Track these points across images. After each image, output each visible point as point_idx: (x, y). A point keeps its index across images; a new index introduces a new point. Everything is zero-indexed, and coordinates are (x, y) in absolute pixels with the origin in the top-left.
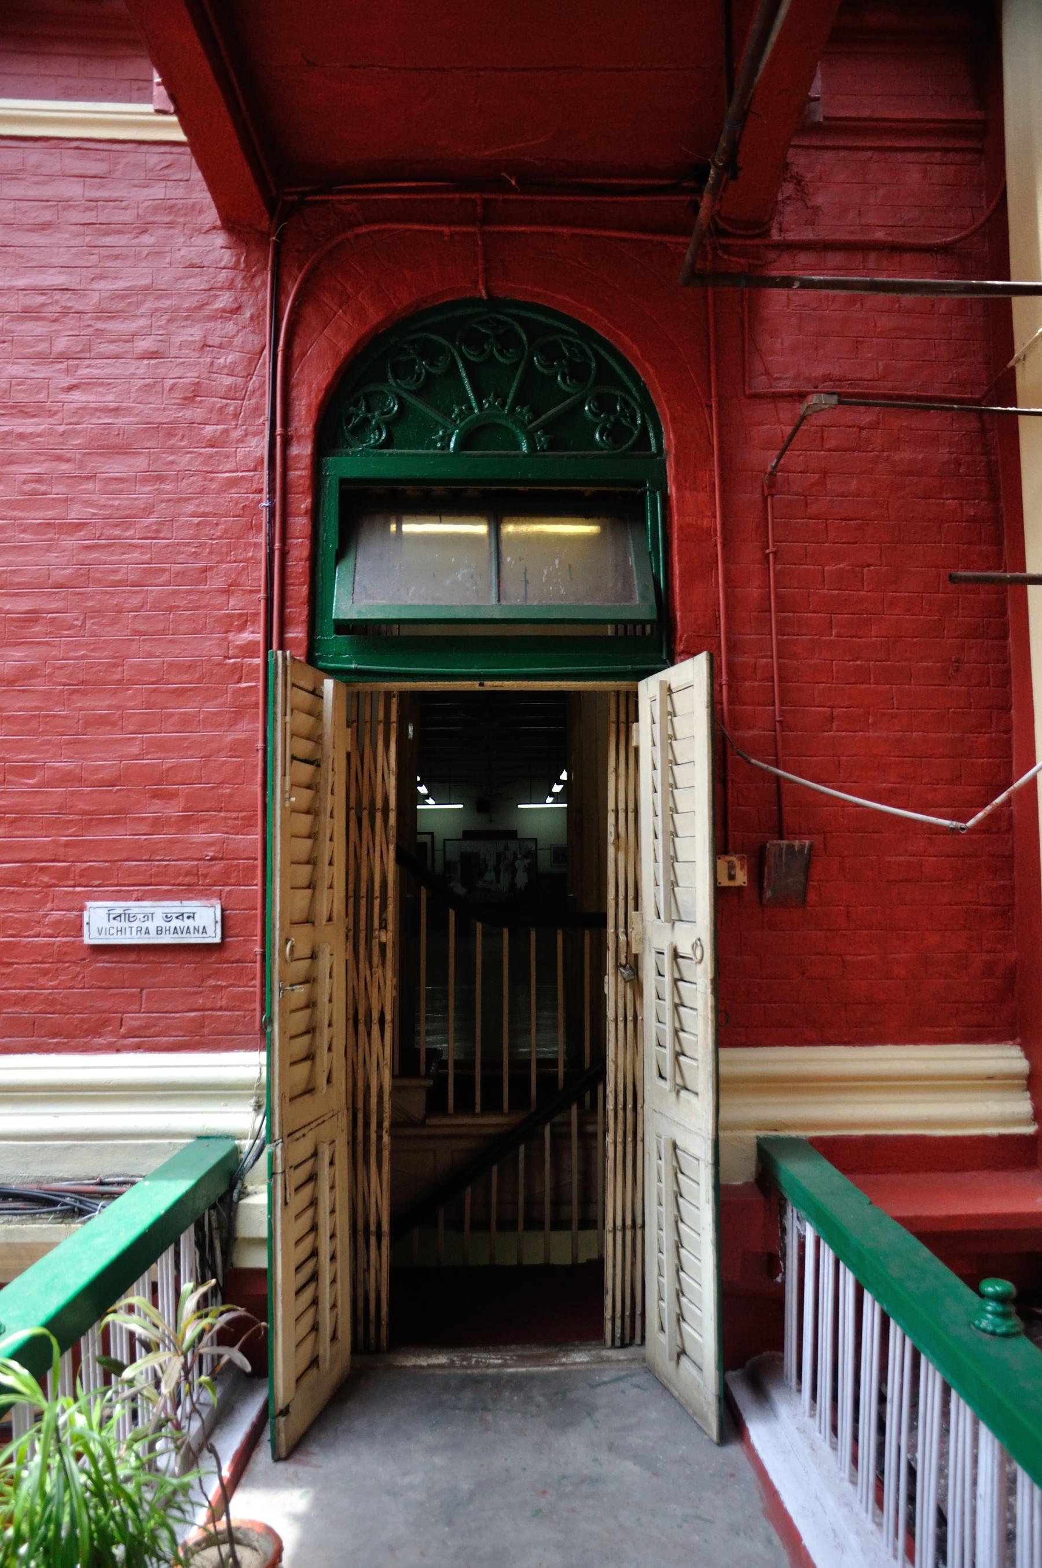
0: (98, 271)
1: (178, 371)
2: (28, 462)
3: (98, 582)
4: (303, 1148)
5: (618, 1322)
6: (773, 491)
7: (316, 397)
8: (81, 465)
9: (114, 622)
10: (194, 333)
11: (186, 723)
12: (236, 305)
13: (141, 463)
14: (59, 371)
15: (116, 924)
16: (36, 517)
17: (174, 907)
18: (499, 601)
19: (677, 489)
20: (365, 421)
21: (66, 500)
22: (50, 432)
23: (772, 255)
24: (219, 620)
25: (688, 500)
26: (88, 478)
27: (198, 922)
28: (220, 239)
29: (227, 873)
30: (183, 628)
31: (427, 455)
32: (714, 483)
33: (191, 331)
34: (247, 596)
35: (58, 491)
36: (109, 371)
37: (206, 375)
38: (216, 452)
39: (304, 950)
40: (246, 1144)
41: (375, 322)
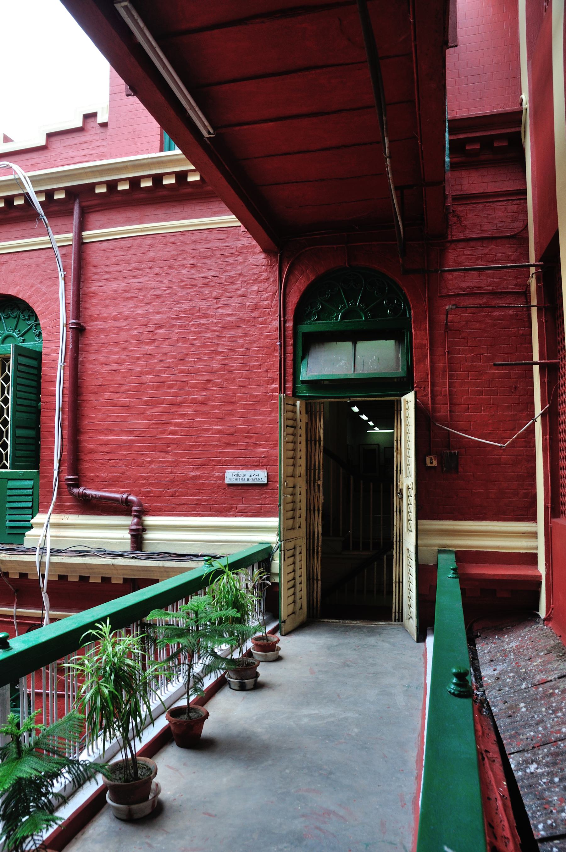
0: (225, 269)
1: (251, 300)
2: (205, 332)
3: (228, 370)
4: (290, 545)
5: (397, 614)
8: (222, 333)
9: (233, 383)
10: (255, 288)
11: (255, 414)
13: (240, 331)
14: (214, 303)
15: (235, 477)
16: (208, 350)
17: (252, 472)
20: (311, 312)
21: (217, 344)
22: (212, 323)
23: (448, 244)
24: (265, 381)
26: (224, 337)
27: (260, 477)
28: (263, 255)
29: (268, 461)
30: (254, 384)
31: (331, 323)
33: (254, 287)
35: (215, 342)
36: (229, 302)
39: (291, 485)
40: (274, 546)
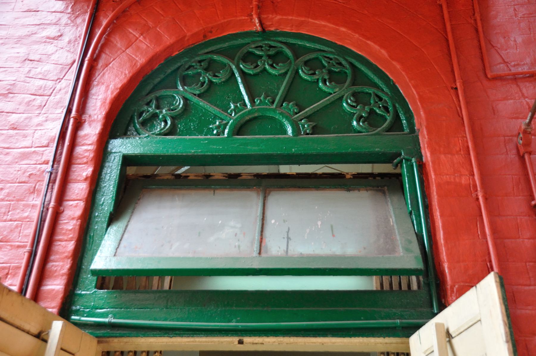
6: (529, 149)
7: (112, 93)
12: (59, 34)
18: (260, 253)
19: (432, 153)
25: (442, 162)
32: (468, 147)
34: (14, 251)
37: (22, 79)
38: (16, 134)
41: (168, 43)
